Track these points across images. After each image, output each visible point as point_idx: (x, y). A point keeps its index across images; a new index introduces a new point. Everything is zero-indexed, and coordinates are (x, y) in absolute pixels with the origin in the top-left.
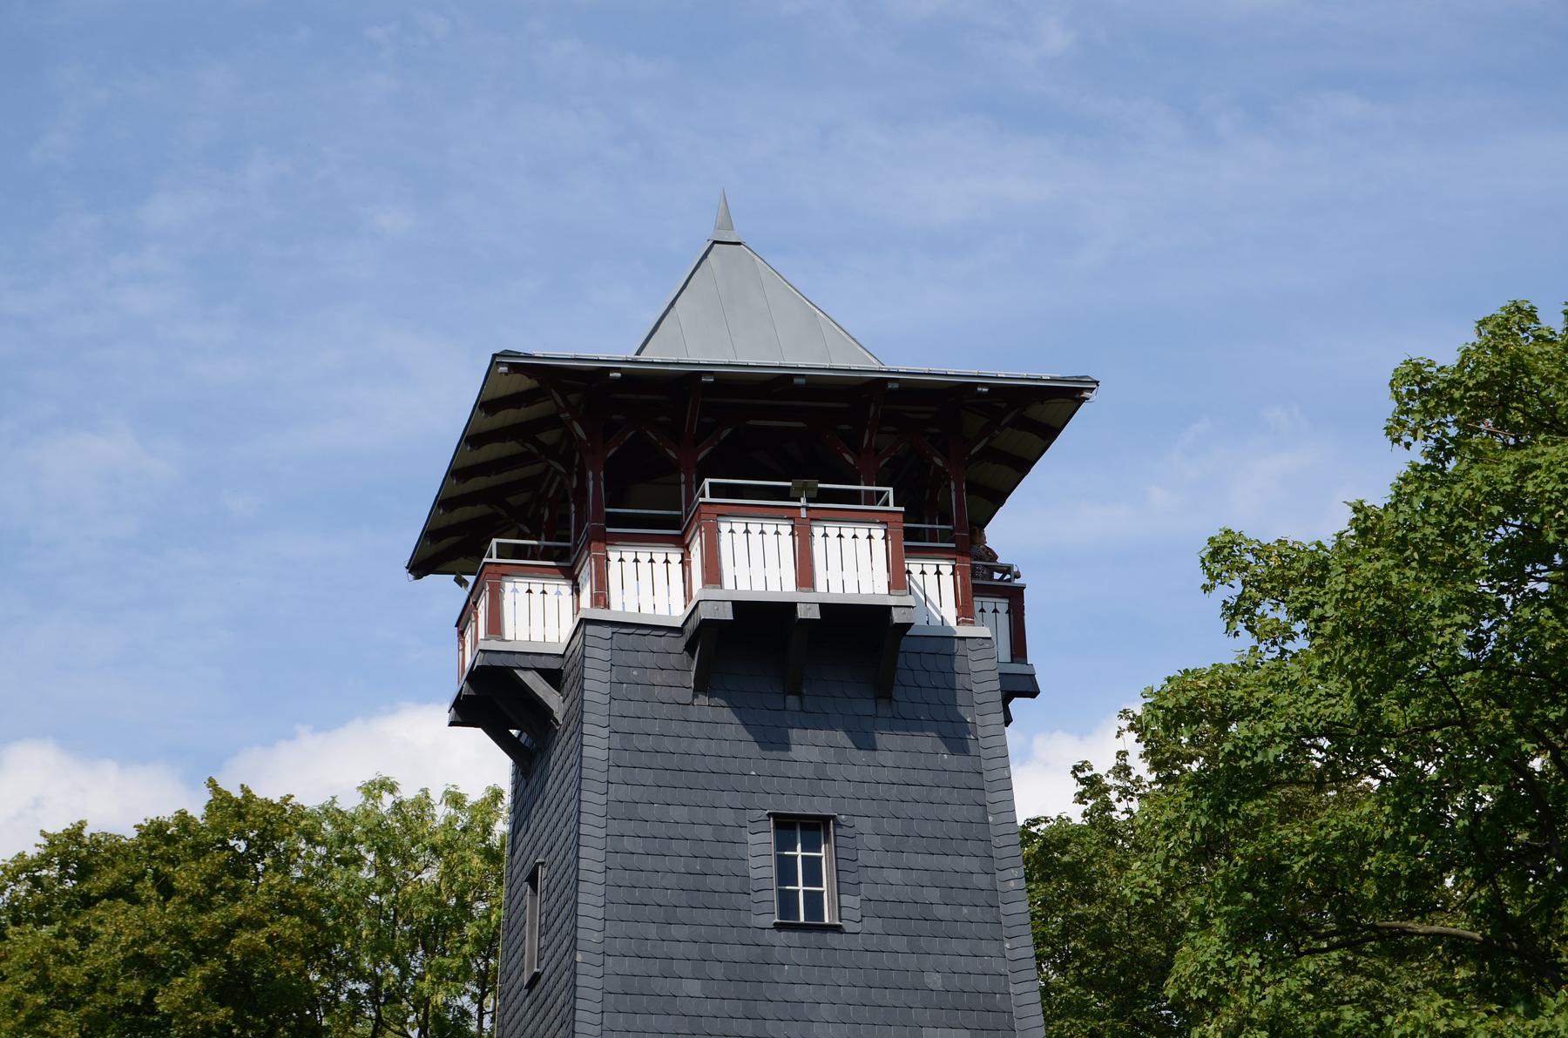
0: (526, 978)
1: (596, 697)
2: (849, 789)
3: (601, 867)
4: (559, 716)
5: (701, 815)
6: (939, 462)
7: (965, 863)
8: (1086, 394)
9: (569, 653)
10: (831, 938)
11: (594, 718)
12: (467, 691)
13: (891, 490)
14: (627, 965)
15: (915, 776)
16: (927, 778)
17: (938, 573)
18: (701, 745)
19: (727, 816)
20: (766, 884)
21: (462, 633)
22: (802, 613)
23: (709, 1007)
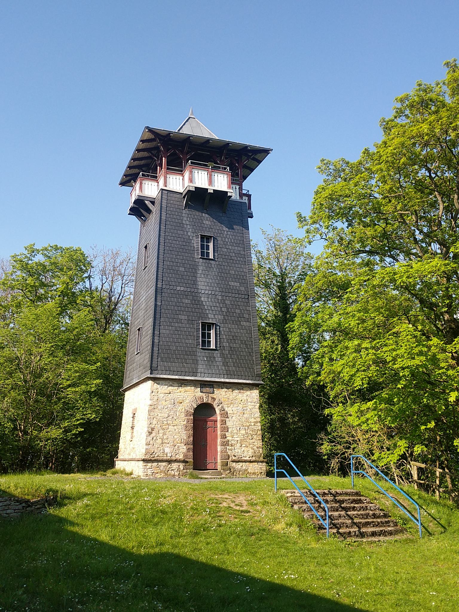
8: (270, 152)
10: (212, 262)
17: (236, 188)
21: (202, 478)
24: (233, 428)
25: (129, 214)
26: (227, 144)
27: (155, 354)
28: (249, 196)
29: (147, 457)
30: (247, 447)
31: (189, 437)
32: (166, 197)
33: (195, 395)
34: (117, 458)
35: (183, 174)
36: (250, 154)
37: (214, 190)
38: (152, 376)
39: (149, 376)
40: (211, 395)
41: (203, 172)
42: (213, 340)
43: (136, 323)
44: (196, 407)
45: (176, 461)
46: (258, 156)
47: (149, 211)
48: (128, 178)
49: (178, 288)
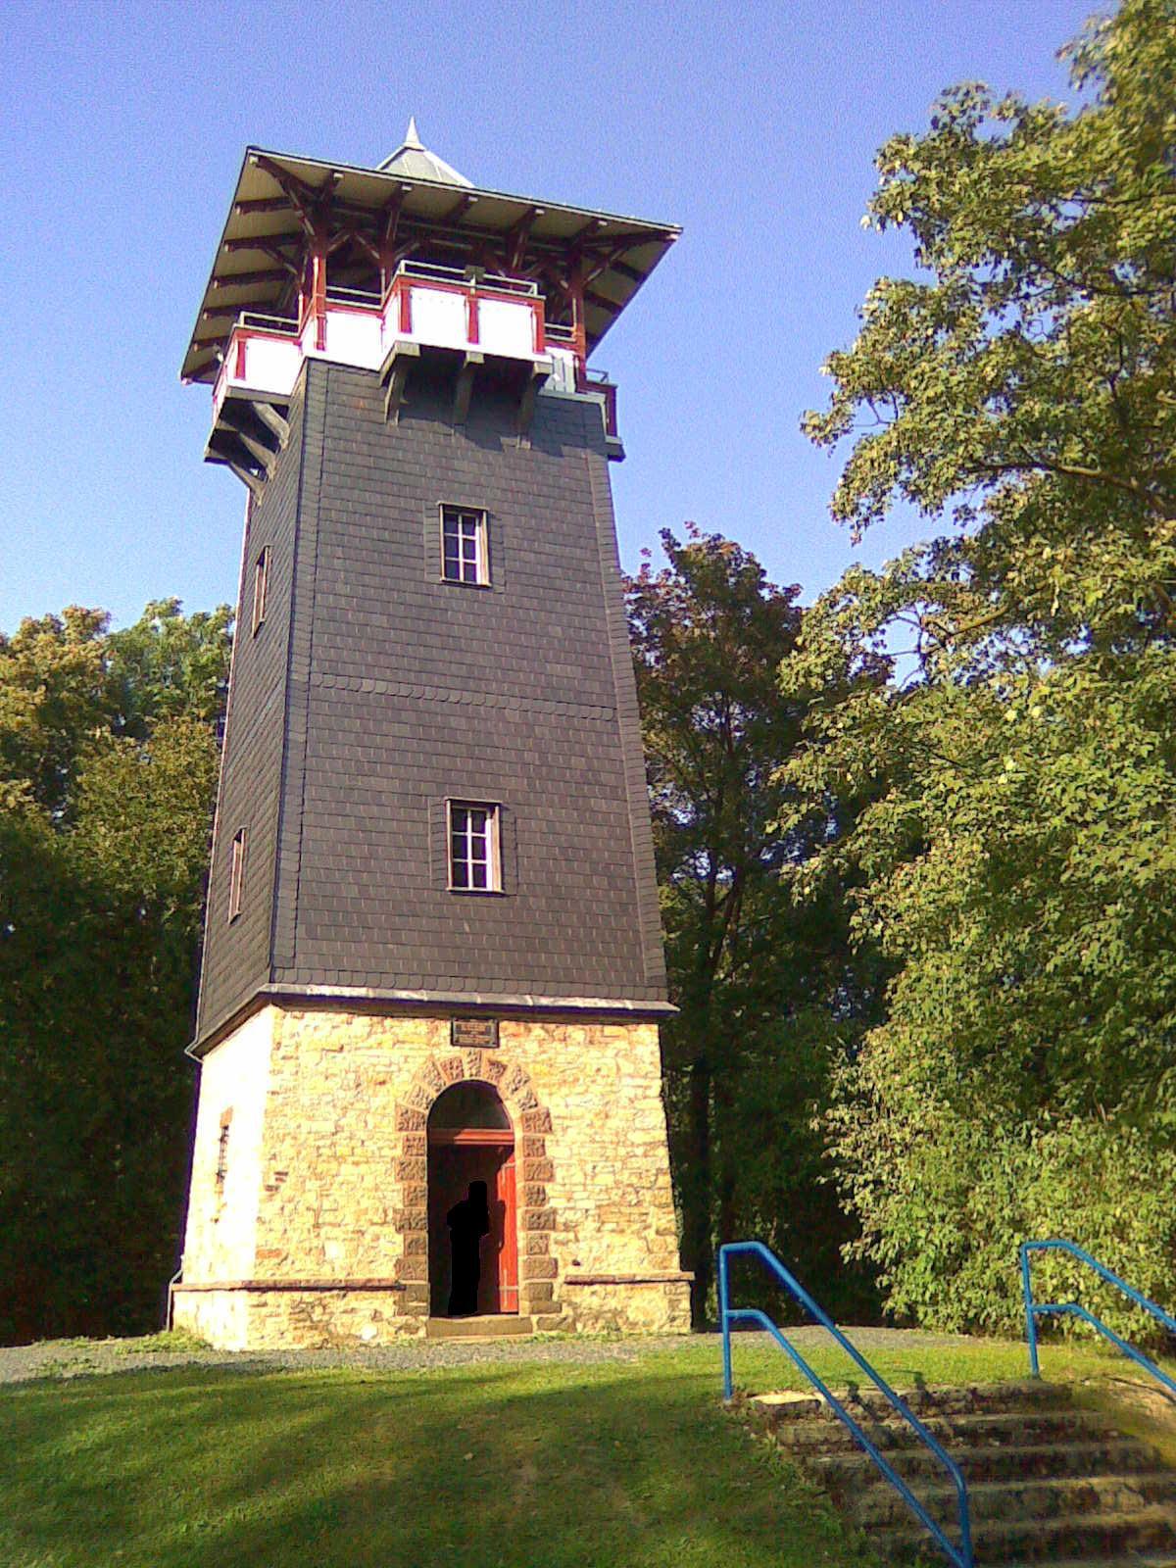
0: (230, 918)
1: (316, 412)
6: (565, 285)
24: (570, 1166)
25: (207, 460)
26: (530, 213)
27: (286, 911)
28: (610, 391)
29: (264, 1275)
30: (622, 1231)
31: (412, 1202)
32: (324, 383)
33: (432, 1056)
34: (179, 1281)
36: (606, 250)
38: (275, 988)
39: (264, 988)
40: (488, 1054)
42: (491, 861)
44: (434, 1095)
45: (368, 1287)
46: (634, 256)
47: (270, 440)
49: (367, 685)
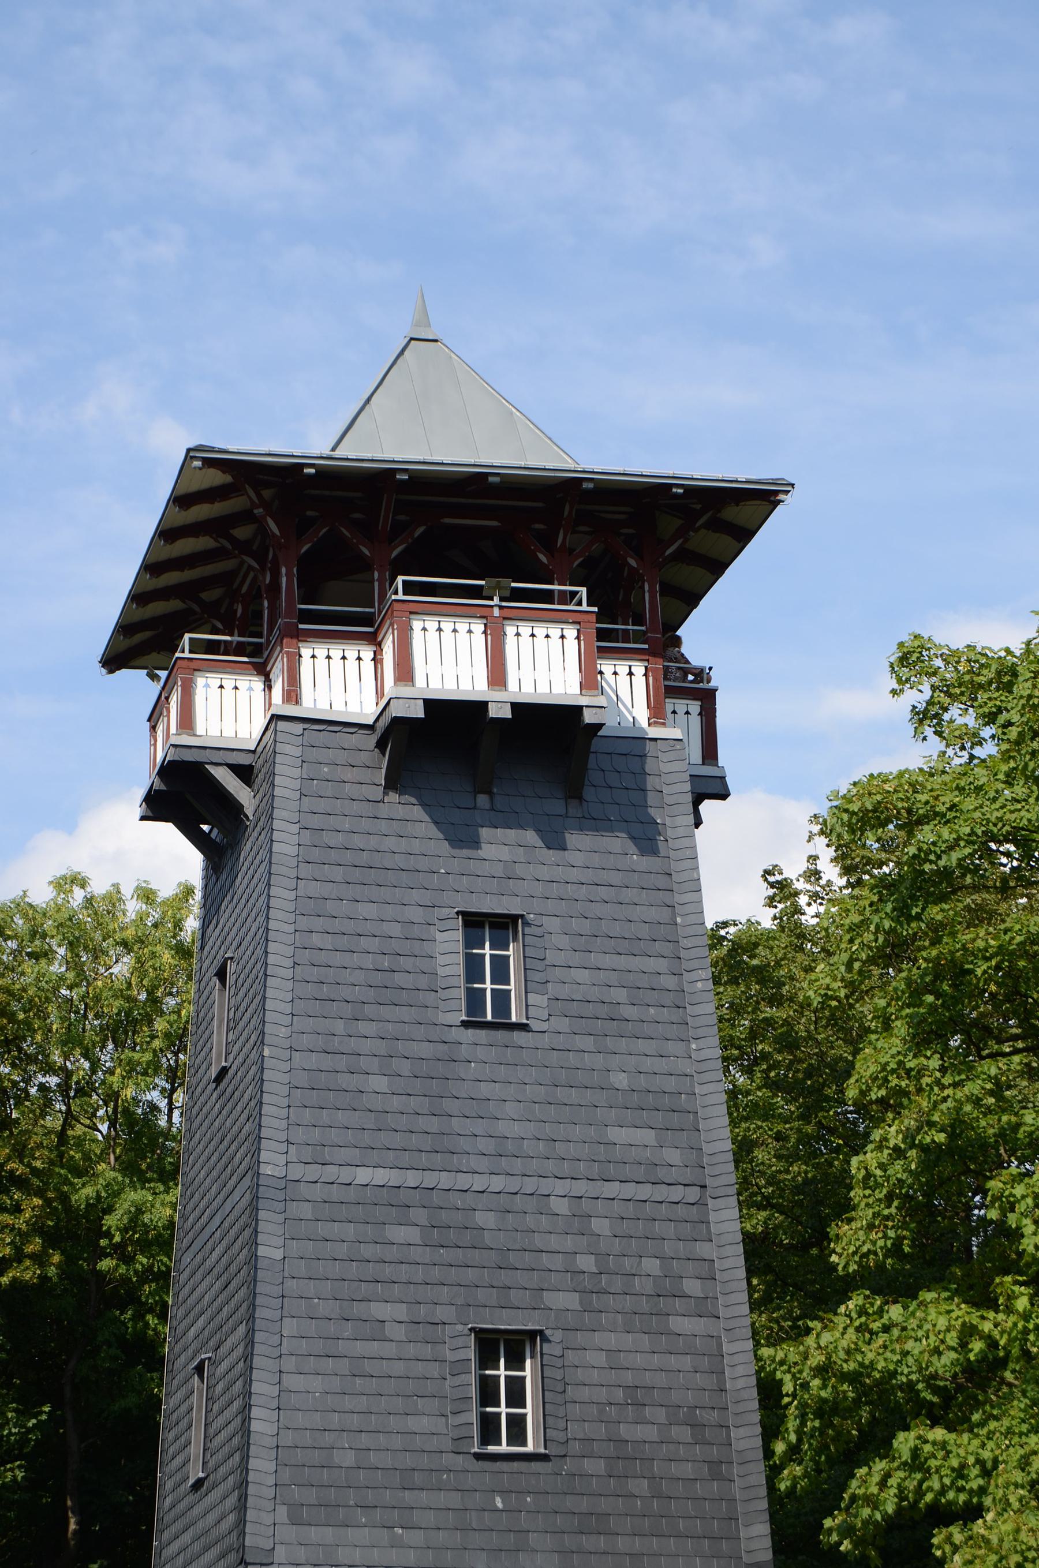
0: (191, 1481)
1: (287, 793)
2: (539, 889)
3: (289, 963)
4: (249, 812)
5: (390, 912)
7: (652, 964)
9: (260, 749)
10: (518, 1036)
11: (284, 814)
12: (159, 785)
13: (584, 590)
14: (314, 1060)
15: (604, 876)
16: (615, 878)
17: (631, 674)
18: (390, 843)
19: (416, 914)
20: (453, 982)
21: (153, 728)
22: (493, 712)
23: (396, 1102)
35: (375, 634)
37: (515, 706)
41: (462, 626)
43: (192, 1332)
46: (732, 513)
48: (139, 637)
